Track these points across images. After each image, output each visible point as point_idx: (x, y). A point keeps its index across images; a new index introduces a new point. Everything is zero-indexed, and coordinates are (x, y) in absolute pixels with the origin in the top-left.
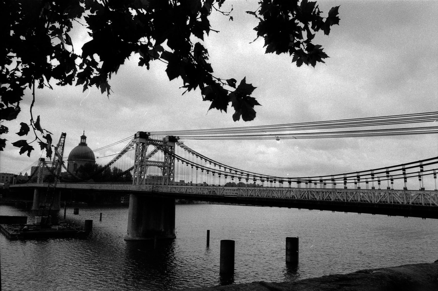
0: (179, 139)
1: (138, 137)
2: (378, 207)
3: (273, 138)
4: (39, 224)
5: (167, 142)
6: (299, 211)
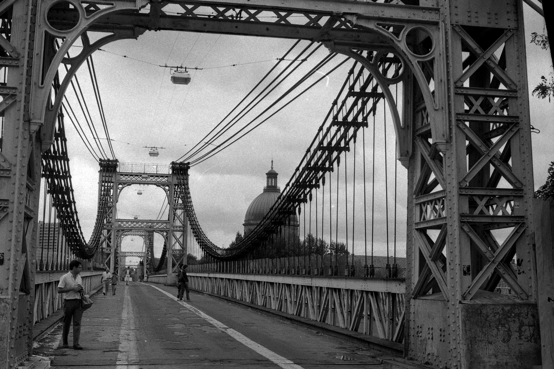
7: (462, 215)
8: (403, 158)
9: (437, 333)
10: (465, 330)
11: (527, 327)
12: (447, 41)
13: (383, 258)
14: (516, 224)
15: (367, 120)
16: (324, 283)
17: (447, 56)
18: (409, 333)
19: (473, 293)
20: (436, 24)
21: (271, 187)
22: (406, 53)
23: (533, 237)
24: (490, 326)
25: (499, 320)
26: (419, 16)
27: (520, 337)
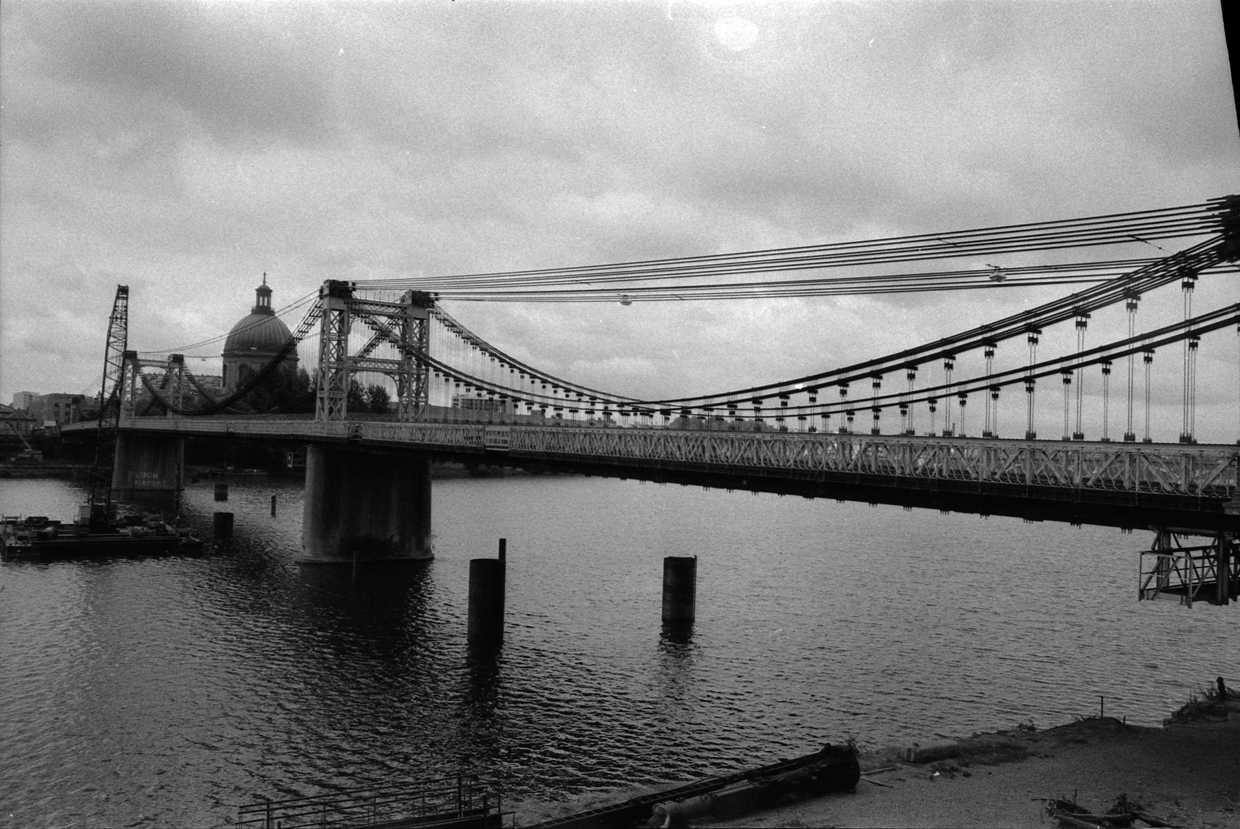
0: (437, 299)
1: (327, 295)
2: (766, 476)
3: (608, 299)
4: (87, 523)
6: (705, 492)
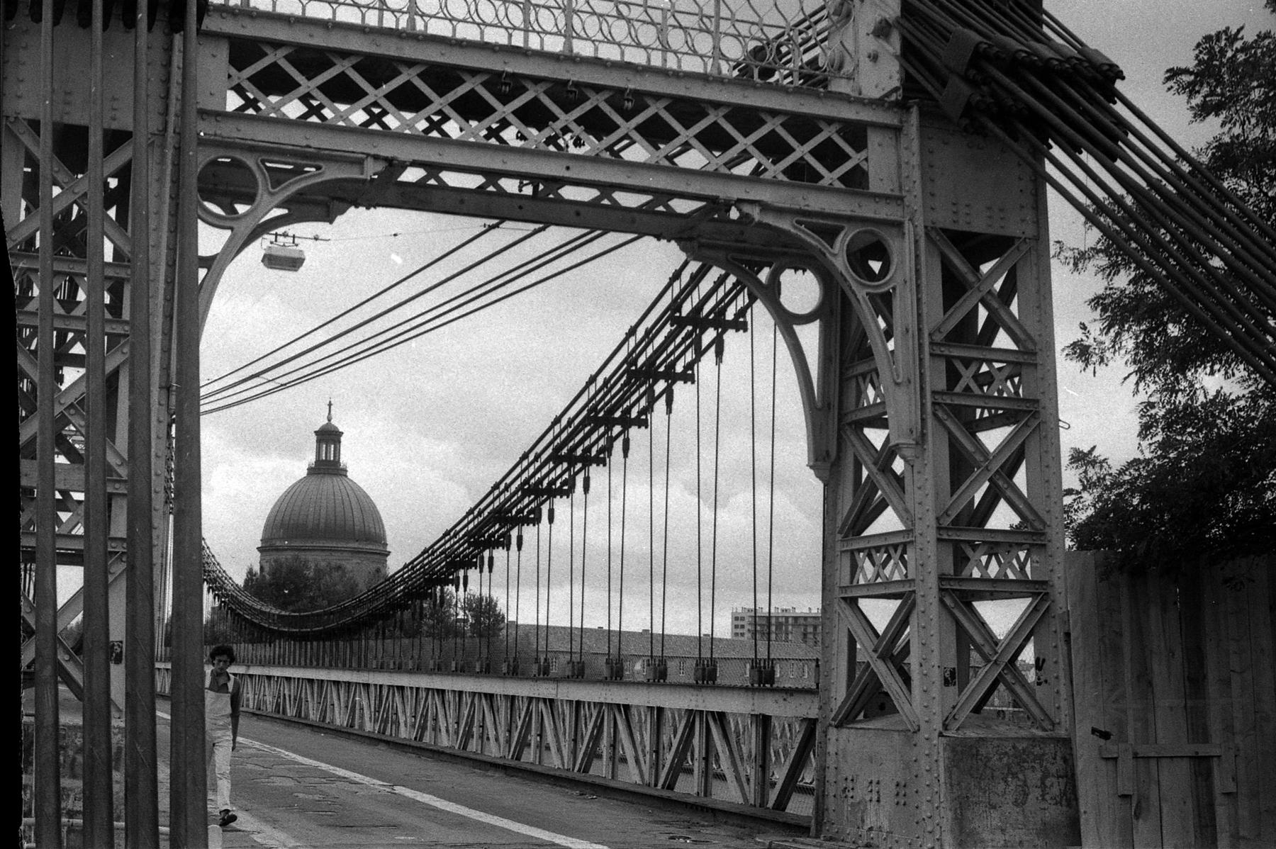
5: (856, 134)
7: (942, 578)
8: (819, 463)
9: (888, 791)
10: (951, 785)
11: (1054, 780)
12: (917, 256)
13: (564, 628)
14: (1034, 595)
15: (692, 369)
16: (423, 682)
17: (918, 286)
18: (824, 791)
19: (962, 718)
20: (899, 225)
21: (327, 462)
22: (848, 277)
23: (1066, 618)
24: (993, 777)
25: (1009, 766)
26: (868, 210)
27: (1043, 796)
